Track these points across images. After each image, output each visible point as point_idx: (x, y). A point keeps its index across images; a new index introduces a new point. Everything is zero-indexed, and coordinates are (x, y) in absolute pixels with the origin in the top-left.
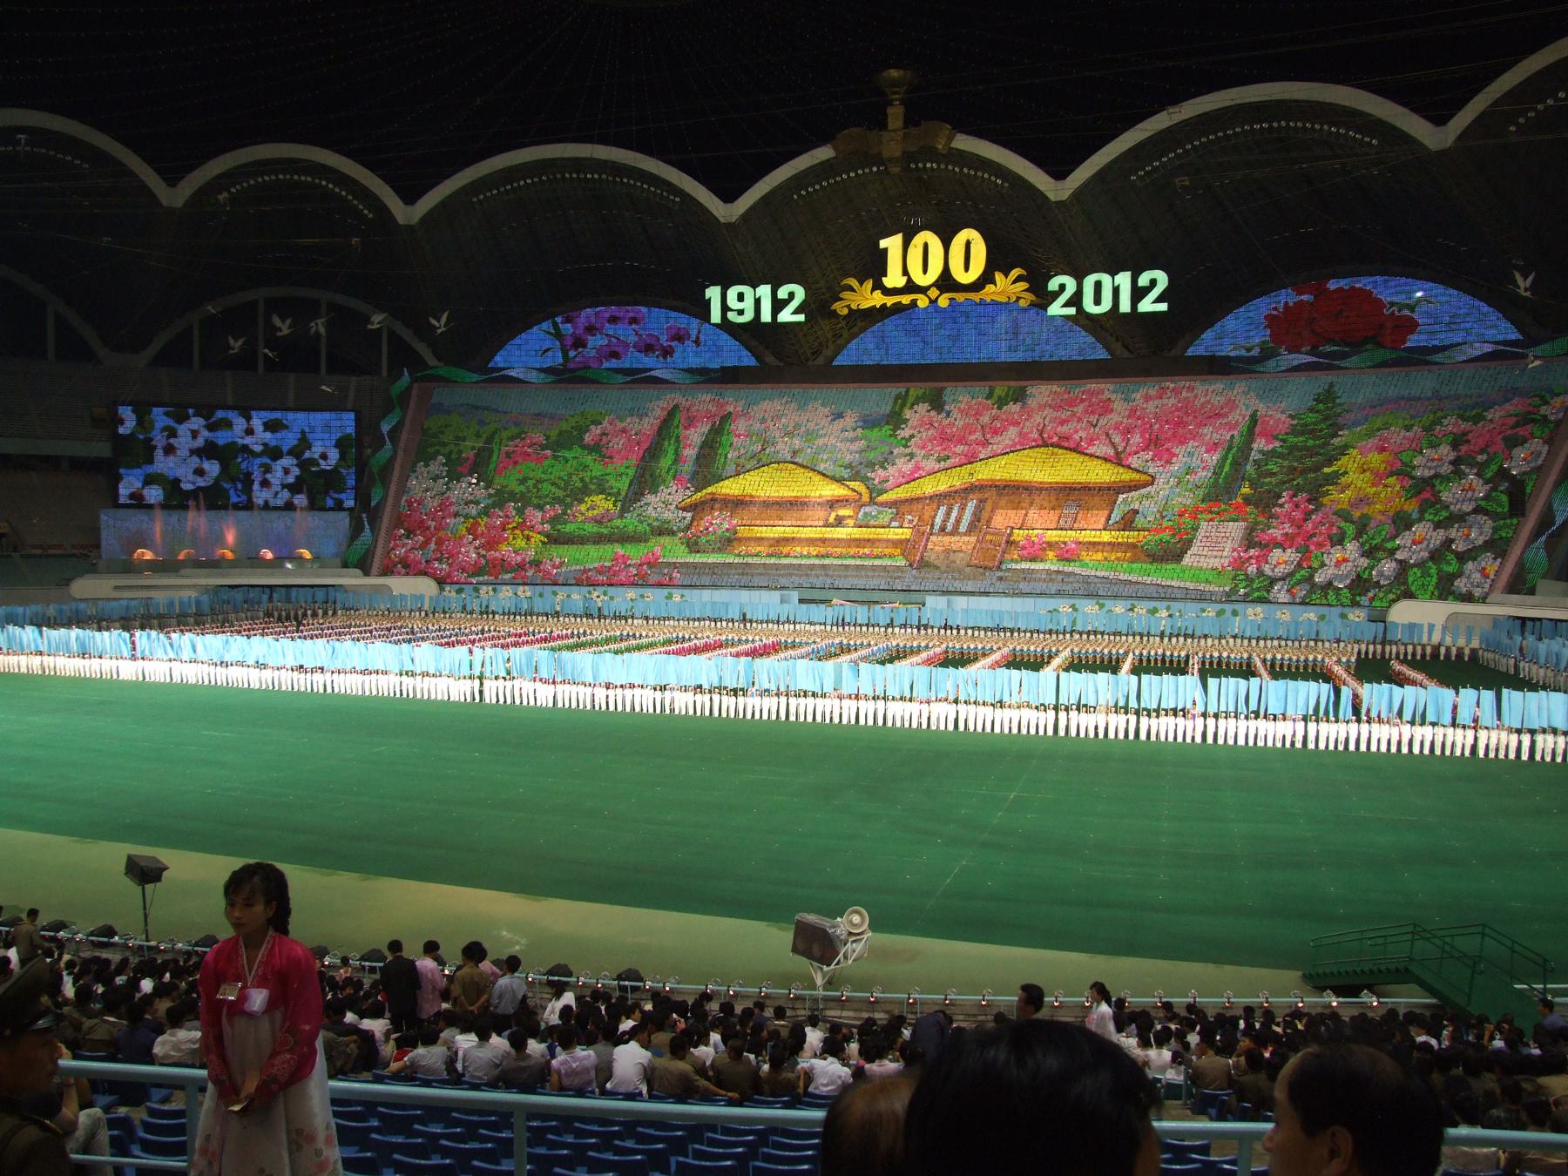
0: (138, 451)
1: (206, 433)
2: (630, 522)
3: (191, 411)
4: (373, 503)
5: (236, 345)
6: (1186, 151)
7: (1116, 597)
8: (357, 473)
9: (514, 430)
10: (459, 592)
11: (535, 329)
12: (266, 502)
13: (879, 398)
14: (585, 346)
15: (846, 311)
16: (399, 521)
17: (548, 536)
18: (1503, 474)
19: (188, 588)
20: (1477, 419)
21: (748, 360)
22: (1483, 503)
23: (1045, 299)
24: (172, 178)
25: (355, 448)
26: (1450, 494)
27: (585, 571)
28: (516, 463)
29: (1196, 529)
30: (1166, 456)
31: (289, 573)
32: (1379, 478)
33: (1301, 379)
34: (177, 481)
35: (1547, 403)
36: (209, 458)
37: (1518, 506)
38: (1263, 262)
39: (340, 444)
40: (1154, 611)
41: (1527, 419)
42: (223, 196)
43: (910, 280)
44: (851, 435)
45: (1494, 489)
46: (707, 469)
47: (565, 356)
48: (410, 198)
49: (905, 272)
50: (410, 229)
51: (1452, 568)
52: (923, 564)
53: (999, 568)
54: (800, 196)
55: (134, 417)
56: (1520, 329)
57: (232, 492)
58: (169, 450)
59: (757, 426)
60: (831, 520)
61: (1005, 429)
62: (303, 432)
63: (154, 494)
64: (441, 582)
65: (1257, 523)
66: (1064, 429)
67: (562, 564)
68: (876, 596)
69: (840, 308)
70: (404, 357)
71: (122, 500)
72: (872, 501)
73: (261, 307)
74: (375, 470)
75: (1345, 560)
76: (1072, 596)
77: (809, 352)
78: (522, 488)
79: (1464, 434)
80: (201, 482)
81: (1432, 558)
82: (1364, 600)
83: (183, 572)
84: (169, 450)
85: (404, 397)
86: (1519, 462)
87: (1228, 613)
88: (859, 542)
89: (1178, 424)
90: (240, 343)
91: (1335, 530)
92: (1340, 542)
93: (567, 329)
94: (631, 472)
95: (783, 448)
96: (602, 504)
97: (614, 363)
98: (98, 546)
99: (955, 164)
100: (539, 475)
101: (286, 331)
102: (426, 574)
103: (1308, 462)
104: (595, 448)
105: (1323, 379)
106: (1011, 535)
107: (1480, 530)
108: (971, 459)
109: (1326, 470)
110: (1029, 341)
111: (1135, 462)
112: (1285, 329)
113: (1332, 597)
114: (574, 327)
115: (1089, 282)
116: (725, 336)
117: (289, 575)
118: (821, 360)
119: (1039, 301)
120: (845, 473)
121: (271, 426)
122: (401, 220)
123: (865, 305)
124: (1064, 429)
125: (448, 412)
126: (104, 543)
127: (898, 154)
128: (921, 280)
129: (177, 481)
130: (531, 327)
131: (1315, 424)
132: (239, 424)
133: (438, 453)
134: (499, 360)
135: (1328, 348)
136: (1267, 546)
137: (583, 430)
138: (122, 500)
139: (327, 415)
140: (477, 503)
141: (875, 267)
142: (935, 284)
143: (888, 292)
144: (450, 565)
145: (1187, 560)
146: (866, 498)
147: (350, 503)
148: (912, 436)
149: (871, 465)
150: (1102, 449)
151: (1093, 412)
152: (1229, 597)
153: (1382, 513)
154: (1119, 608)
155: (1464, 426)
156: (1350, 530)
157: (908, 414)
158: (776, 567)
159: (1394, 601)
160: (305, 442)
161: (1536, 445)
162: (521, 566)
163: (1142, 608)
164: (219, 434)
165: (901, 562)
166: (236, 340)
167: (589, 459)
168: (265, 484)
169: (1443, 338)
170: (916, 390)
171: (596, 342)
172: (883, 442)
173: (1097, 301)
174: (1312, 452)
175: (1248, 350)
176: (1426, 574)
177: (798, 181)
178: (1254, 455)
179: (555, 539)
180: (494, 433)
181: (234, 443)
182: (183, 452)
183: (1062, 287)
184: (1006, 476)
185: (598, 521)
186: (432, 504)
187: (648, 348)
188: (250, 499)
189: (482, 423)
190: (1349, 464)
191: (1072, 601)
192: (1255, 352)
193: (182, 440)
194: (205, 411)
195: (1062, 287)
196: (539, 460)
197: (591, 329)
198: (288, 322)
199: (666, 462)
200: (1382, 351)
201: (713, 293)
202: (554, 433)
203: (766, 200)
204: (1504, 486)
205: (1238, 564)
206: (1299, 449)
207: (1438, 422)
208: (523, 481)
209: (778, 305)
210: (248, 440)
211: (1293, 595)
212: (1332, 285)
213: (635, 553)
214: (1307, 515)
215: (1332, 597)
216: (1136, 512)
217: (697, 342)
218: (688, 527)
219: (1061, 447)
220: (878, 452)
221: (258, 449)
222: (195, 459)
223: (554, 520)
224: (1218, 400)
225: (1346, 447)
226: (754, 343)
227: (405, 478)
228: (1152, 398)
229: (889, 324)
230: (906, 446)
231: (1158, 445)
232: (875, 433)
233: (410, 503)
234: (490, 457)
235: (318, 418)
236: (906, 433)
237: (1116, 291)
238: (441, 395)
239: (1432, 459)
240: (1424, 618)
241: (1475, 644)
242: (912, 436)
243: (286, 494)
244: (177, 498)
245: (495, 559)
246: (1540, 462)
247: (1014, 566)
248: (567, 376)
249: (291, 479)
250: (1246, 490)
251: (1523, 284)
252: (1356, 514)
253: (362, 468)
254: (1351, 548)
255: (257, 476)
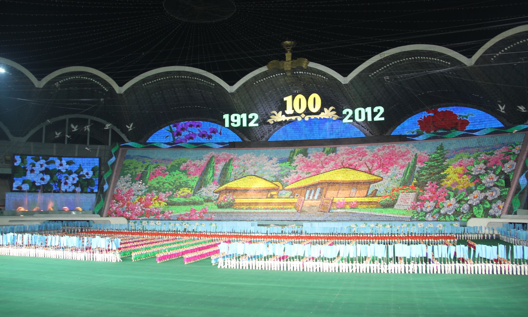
0: (21, 171)
1: (45, 165)
2: (196, 198)
3: (41, 157)
4: (105, 190)
5: (58, 134)
6: (387, 67)
7: (370, 221)
8: (99, 180)
9: (155, 165)
10: (135, 223)
11: (163, 129)
12: (66, 190)
13: (285, 152)
14: (181, 135)
15: (272, 122)
16: (113, 197)
17: (167, 203)
18: (502, 172)
19: (37, 221)
20: (492, 154)
21: (238, 139)
22: (496, 183)
23: (342, 116)
24: (40, 78)
25: (99, 171)
26: (486, 180)
27: (180, 215)
28: (156, 177)
29: (398, 196)
30: (386, 171)
31: (74, 216)
32: (460, 176)
33: (430, 142)
34: (34, 182)
35: (514, 148)
36: (46, 174)
37: (508, 184)
38: (415, 104)
39: (93, 169)
40: (385, 225)
41: (508, 154)
42: (57, 84)
43: (295, 111)
44: (275, 165)
45: (500, 178)
46: (224, 178)
47: (174, 139)
48: (121, 85)
49: (293, 109)
50: (121, 95)
51: (488, 206)
52: (302, 211)
53: (329, 212)
54: (256, 83)
55: (20, 159)
56: (503, 123)
57: (54, 187)
58: (32, 171)
59: (242, 163)
60: (269, 196)
61: (330, 162)
62: (80, 165)
63: (26, 187)
64: (129, 219)
65: (419, 193)
66: (350, 162)
67: (172, 213)
68: (285, 223)
69: (270, 121)
70: (117, 139)
71: (14, 189)
72: (283, 189)
73: (67, 121)
74: (105, 179)
75: (451, 205)
76: (355, 221)
77: (260, 136)
78: (158, 185)
79: (488, 159)
80: (43, 183)
81: (481, 203)
82: (458, 218)
83: (35, 215)
84: (32, 171)
85: (116, 153)
86: (507, 168)
87: (411, 225)
88: (279, 204)
89: (390, 159)
90: (59, 134)
91: (446, 195)
92: (449, 199)
93: (175, 129)
94: (197, 179)
95: (251, 171)
96: (187, 191)
97: (191, 141)
98: (4, 206)
99: (309, 72)
100: (164, 180)
101: (75, 130)
102: (123, 216)
103: (436, 170)
104: (184, 171)
105: (440, 142)
106: (333, 200)
107: (496, 193)
108: (318, 173)
109: (442, 173)
110: (337, 131)
111: (376, 172)
112: (424, 125)
113: (447, 217)
114: (177, 128)
115: (357, 111)
116: (230, 131)
117: (74, 216)
118: (264, 139)
119: (340, 117)
120: (273, 179)
121: (68, 163)
122: (118, 92)
123: (279, 120)
124: (350, 162)
125: (132, 158)
126: (6, 205)
127: (289, 69)
128: (298, 111)
129: (34, 182)
130: (162, 128)
131: (438, 157)
132: (58, 162)
133: (128, 173)
134: (150, 140)
135: (440, 131)
136: (424, 201)
137: (179, 165)
138: (14, 189)
139: (89, 159)
140: (142, 191)
141: (282, 107)
142: (304, 113)
143: (287, 115)
144: (132, 213)
145: (395, 207)
146: (281, 188)
147: (96, 191)
148: (297, 166)
149: (283, 176)
150: (363, 168)
151: (360, 156)
152: (411, 219)
153: (462, 188)
154: (372, 225)
155: (488, 156)
156: (452, 194)
157: (295, 158)
158: (250, 213)
159: (469, 219)
160: (81, 169)
161: (511, 162)
162: (158, 214)
163: (381, 224)
164: (50, 165)
165: (294, 210)
166: (58, 133)
167: (182, 175)
168: (66, 183)
169: (478, 127)
170: (297, 149)
171: (185, 133)
172: (287, 168)
173: (360, 118)
174: (437, 167)
175: (413, 133)
176: (479, 208)
177: (255, 78)
178: (417, 169)
179: (170, 204)
180: (148, 166)
181: (55, 169)
182: (37, 172)
183: (348, 113)
184: (331, 179)
185: (185, 197)
186: (125, 191)
187: (203, 136)
188: (60, 189)
189: (144, 162)
190: (450, 171)
191: (356, 223)
192: (415, 133)
193: (37, 168)
194: (46, 157)
195: (348, 113)
196: (164, 176)
197: (183, 129)
198: (77, 126)
199: (210, 175)
200: (458, 132)
201: (226, 117)
202: (169, 166)
203: (244, 85)
204: (503, 177)
205: (414, 207)
206: (432, 166)
207: (478, 156)
208: (158, 183)
209: (249, 121)
210: (60, 168)
211: (434, 218)
212: (439, 110)
213: (198, 208)
214: (437, 189)
215: (447, 217)
216: (377, 190)
217: (220, 133)
218: (218, 199)
219: (350, 168)
220: (284, 172)
221: (64, 171)
222: (41, 174)
223: (169, 197)
224: (403, 150)
225: (448, 165)
226: (240, 134)
227: (116, 182)
228: (379, 150)
229: (287, 127)
230: (295, 169)
231: (384, 166)
232: (283, 165)
233: (117, 191)
234: (147, 174)
235: (86, 160)
236: (295, 164)
237: (366, 114)
238: (129, 152)
239: (477, 168)
240: (480, 224)
241: (496, 232)
242: (297, 166)
243: (73, 187)
244: (34, 188)
245: (148, 211)
246: (514, 168)
247: (334, 211)
248: (174, 145)
249: (75, 182)
250: (415, 181)
251: (502, 109)
252: (454, 188)
253: (101, 178)
254: (452, 200)
255: (63, 181)
